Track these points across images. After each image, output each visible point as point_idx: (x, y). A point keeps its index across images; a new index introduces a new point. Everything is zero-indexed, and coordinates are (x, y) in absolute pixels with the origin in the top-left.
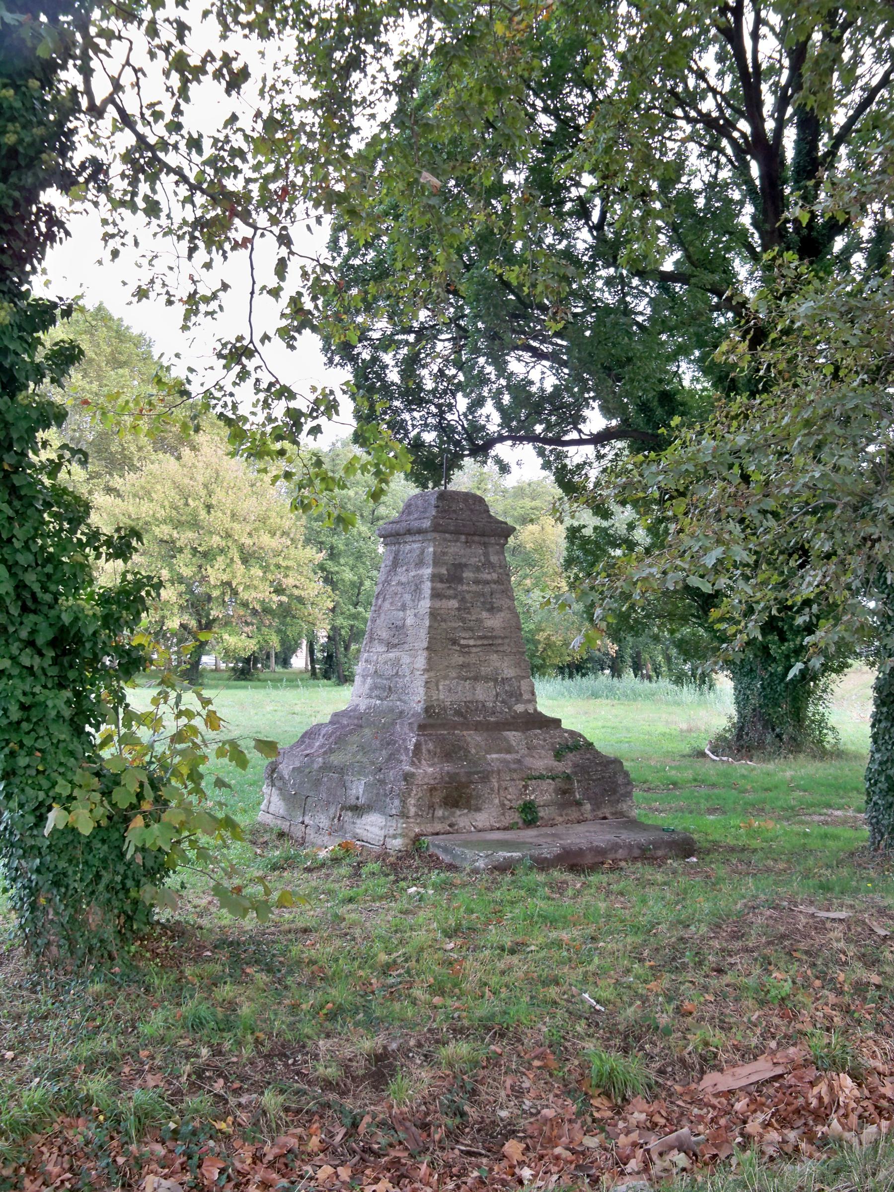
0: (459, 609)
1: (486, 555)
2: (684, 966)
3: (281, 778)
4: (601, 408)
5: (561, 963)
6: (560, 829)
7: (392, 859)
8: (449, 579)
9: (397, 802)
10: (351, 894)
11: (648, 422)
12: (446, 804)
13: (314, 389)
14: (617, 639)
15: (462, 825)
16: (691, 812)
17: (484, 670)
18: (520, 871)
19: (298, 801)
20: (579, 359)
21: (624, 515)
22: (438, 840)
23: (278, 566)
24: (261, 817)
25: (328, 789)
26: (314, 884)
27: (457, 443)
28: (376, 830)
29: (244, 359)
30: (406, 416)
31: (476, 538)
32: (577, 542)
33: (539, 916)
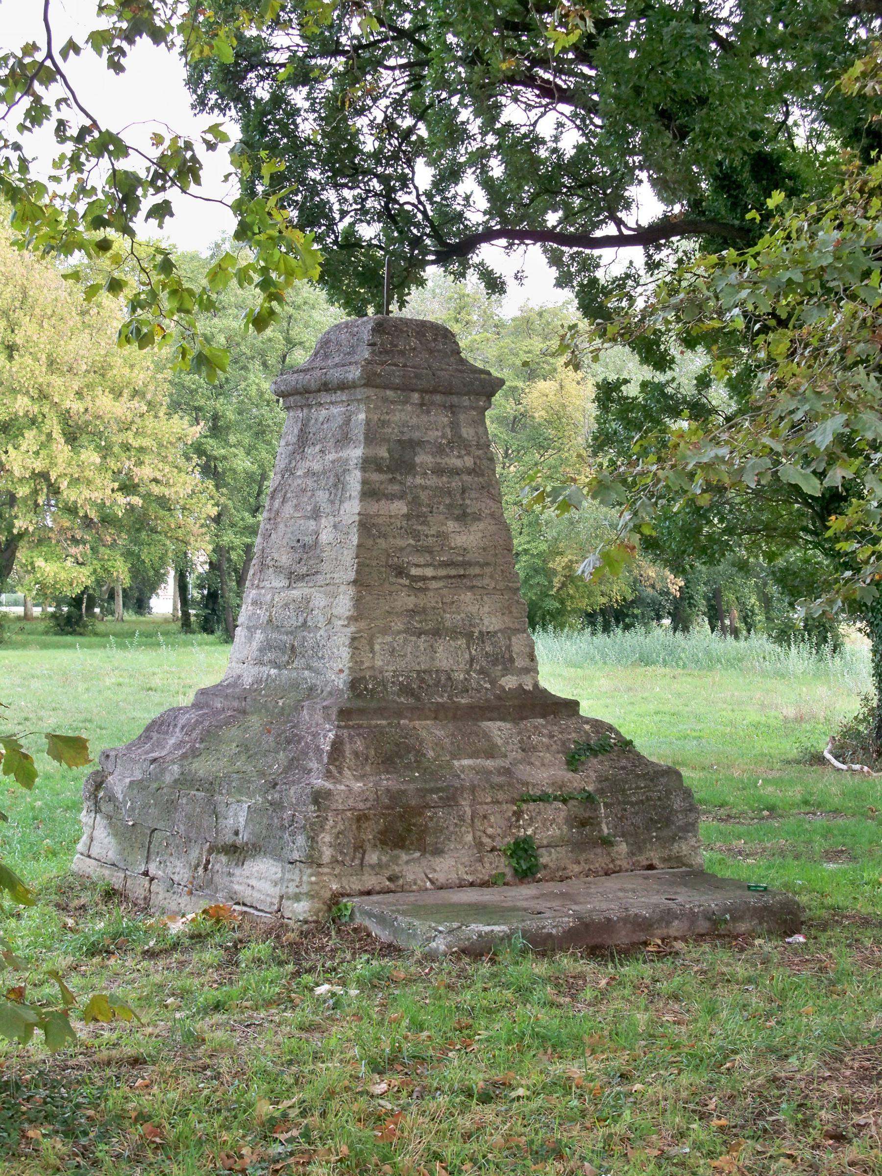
0: (408, 517)
1: (455, 425)
2: (778, 1129)
3: (111, 798)
4: (654, 182)
5: (567, 1119)
6: (575, 886)
7: (292, 936)
8: (391, 465)
9: (301, 840)
10: (219, 995)
11: (734, 206)
12: (384, 843)
13: (158, 140)
14: (678, 570)
15: (410, 877)
16: (797, 857)
17: (451, 619)
18: (505, 957)
19: (138, 838)
20: (616, 98)
21: (691, 363)
22: (367, 903)
23: (126, 447)
24: (78, 863)
25: (189, 817)
26: (157, 978)
27: (416, 242)
28: (266, 887)
29: (36, 85)
30: (330, 195)
31: (438, 398)
32: (614, 407)
33: (536, 1035)
